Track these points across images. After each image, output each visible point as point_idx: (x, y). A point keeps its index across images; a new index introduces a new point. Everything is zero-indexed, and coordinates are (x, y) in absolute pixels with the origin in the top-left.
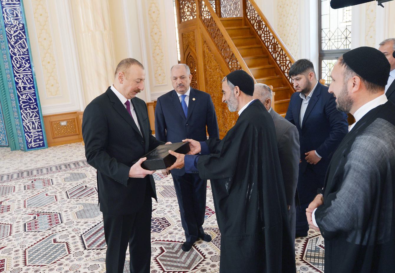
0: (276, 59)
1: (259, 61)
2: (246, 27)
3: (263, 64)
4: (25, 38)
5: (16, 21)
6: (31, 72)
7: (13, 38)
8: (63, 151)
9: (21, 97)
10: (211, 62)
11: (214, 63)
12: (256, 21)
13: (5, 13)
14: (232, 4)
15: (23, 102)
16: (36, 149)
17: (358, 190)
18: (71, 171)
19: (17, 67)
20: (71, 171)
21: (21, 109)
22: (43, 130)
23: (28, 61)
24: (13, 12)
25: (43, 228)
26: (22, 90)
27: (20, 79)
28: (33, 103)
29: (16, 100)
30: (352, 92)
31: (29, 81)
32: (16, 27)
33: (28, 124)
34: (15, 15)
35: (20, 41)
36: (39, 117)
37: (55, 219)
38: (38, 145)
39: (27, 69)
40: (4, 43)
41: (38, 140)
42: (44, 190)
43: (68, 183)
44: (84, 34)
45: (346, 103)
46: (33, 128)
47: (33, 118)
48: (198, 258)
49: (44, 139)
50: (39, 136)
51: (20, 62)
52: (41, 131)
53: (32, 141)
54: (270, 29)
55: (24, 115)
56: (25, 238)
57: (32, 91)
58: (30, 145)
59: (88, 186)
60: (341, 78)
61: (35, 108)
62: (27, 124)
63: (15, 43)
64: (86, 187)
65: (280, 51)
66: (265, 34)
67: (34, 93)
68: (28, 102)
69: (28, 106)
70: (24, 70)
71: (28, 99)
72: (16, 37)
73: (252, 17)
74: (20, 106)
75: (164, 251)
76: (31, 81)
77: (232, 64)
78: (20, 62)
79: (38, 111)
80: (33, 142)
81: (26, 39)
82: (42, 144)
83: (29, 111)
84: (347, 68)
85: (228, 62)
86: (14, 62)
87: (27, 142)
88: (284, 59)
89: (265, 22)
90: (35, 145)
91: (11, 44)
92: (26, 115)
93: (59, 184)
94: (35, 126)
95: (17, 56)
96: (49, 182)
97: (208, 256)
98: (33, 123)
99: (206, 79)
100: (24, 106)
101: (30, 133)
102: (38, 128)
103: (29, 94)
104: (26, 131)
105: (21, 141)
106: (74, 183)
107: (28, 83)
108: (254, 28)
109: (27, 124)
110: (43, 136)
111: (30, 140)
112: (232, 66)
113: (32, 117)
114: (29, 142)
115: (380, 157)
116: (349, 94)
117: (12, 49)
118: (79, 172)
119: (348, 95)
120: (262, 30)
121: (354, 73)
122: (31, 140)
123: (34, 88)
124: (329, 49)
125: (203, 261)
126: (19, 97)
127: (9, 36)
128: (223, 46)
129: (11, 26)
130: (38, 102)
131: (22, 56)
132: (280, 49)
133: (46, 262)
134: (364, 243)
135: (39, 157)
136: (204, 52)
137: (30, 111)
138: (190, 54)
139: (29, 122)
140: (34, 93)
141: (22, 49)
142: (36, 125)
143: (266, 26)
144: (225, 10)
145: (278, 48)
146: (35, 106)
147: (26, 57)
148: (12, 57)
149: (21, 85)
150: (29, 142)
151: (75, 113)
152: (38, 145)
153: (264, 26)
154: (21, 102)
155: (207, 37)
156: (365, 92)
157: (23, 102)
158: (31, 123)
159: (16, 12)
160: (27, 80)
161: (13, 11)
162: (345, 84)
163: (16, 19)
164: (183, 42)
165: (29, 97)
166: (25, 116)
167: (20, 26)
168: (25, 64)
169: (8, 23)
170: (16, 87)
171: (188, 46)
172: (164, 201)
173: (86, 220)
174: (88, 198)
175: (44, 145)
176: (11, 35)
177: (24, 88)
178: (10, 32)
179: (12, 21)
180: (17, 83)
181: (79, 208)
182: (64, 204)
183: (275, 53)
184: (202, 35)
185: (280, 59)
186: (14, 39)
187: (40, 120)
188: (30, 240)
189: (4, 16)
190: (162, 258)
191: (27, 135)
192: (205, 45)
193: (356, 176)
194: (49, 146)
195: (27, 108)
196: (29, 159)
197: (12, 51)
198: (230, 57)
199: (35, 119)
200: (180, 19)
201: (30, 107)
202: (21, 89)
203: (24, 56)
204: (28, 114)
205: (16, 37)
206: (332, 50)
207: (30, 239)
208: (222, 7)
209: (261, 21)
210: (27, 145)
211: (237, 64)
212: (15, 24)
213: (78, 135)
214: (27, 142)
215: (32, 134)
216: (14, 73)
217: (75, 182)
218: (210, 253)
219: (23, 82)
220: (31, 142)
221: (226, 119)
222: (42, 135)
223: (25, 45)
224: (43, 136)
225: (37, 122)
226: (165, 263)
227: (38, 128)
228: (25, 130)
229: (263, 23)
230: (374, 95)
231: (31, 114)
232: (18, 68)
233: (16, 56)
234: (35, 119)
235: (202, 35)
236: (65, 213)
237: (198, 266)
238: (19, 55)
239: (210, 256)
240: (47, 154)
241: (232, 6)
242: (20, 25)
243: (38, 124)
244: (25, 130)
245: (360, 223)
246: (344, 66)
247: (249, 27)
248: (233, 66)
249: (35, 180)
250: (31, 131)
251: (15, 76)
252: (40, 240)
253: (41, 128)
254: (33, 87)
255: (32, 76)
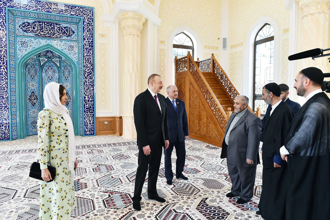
0: (230, 96)
1: (221, 96)
2: (214, 77)
3: (223, 98)
4: (93, 74)
5: (89, 65)
6: (93, 92)
7: (87, 73)
8: (105, 138)
9: (86, 106)
10: (194, 94)
11: (196, 95)
12: (220, 75)
13: (85, 60)
14: (206, 65)
15: (87, 108)
16: (89, 135)
17: (311, 126)
18: (112, 147)
19: (86, 89)
20: (112, 147)
21: (85, 112)
22: (95, 125)
23: (93, 86)
24: (89, 60)
25: (104, 171)
26: (87, 102)
27: (87, 95)
28: (91, 109)
29: (82, 107)
30: (305, 86)
31: (91, 97)
32: (89, 68)
33: (87, 121)
34: (90, 62)
35: (90, 75)
36: (94, 117)
37: (109, 168)
38: (90, 133)
39: (92, 91)
40: (81, 76)
41: (91, 131)
42: (99, 154)
43: (112, 153)
44: (126, 74)
45: (302, 91)
46: (89, 123)
47: (90, 118)
48: (196, 191)
49: (95, 130)
50: (92, 128)
51: (88, 86)
52: (94, 126)
53: (88, 131)
54: (228, 79)
55: (86, 115)
56: (30, 183)
57: (92, 103)
58: (86, 133)
59: (124, 154)
60: (300, 79)
61: (92, 112)
62: (86, 121)
63: (87, 76)
64: (123, 155)
65: (234, 91)
66: (224, 82)
67: (93, 104)
68: (89, 109)
69: (89, 111)
70: (90, 91)
71: (89, 107)
72: (88, 73)
73: (218, 72)
74: (85, 111)
75: (110, 197)
76: (92, 97)
77: (207, 95)
78: (88, 86)
79: (94, 114)
80: (88, 132)
81: (93, 74)
82: (92, 133)
83: (89, 114)
84: (303, 75)
85: (204, 95)
86: (85, 86)
87: (85, 131)
88: (234, 97)
89: (225, 75)
90: (89, 133)
91: (85, 76)
92: (87, 115)
93: (106, 152)
94: (91, 123)
95: (87, 83)
96: (101, 151)
97: (97, 208)
98: (90, 121)
99: (190, 104)
100: (86, 111)
101: (87, 126)
102: (92, 124)
103: (90, 104)
104: (85, 124)
105: (82, 130)
106: (116, 153)
107: (91, 98)
108: (219, 79)
109: (86, 121)
110: (94, 129)
111: (87, 130)
112: (207, 97)
113: (90, 117)
114: (86, 131)
115: (322, 112)
116: (304, 87)
117: (85, 79)
118: (117, 148)
119: (303, 87)
120: (223, 79)
121: (307, 77)
122: (88, 130)
123: (93, 101)
124: (259, 94)
125: (199, 192)
126: (85, 105)
127: (85, 72)
128: (202, 86)
129: (87, 67)
130: (94, 109)
131: (90, 83)
132: (233, 90)
133: (110, 186)
134: (312, 155)
135: (92, 139)
136: (190, 89)
137: (89, 114)
138: (181, 90)
139: (88, 120)
140: (93, 104)
141: (90, 80)
142: (92, 122)
143: (225, 78)
144: (201, 69)
145: (232, 89)
146: (92, 111)
147: (92, 84)
148: (84, 83)
149: (87, 99)
150: (86, 131)
151: (114, 117)
152: (90, 133)
153: (224, 77)
154: (85, 108)
155: (193, 80)
156: (311, 87)
157: (87, 108)
158: (89, 120)
159: (90, 60)
160: (90, 97)
161: (89, 59)
162: (302, 83)
163: (90, 64)
164: (177, 84)
165: (90, 106)
166: (86, 116)
167: (91, 67)
168: (91, 87)
169: (85, 65)
170: (84, 100)
171: (180, 86)
172: (145, 204)
173: (127, 170)
174: (125, 160)
175: (94, 134)
176: (86, 72)
177: (88, 101)
178: (86, 70)
179: (88, 64)
180: (85, 98)
181: (121, 164)
182: (112, 162)
183: (230, 92)
184: (190, 80)
185: (233, 96)
186: (87, 74)
187: (94, 119)
188: (98, 176)
189: (84, 62)
190: (175, 189)
191: (86, 127)
192: (191, 85)
193: (310, 120)
194: (96, 135)
195: (88, 112)
196: (86, 140)
197: (85, 80)
198: (206, 92)
199: (91, 119)
200: (177, 71)
201: (90, 112)
202: (86, 101)
203: (91, 83)
204: (88, 115)
205: (88, 73)
206: (260, 95)
207: (98, 175)
208: (200, 67)
209: (223, 75)
210: (85, 133)
211: (210, 95)
212: (89, 66)
213: (113, 130)
214: (85, 131)
215: (88, 127)
216: (84, 92)
217: (117, 152)
218: (202, 189)
219: (88, 97)
220: (87, 131)
221: (201, 127)
222: (94, 128)
223: (92, 77)
224: (94, 129)
225: (92, 120)
226: (177, 191)
227: (92, 124)
228: (85, 124)
229: (224, 76)
230: (316, 88)
231: (90, 116)
232: (87, 89)
233: (87, 83)
234: (91, 119)
235: (190, 80)
236: (91, 181)
237: (196, 194)
238: (88, 83)
239: (202, 190)
240: (96, 138)
241: (206, 66)
242: (91, 67)
243: (92, 122)
244: (85, 124)
245: (311, 142)
246: (302, 74)
247: (215, 78)
248: (207, 97)
249: (93, 150)
250: (88, 125)
251: (85, 94)
252: (104, 176)
253: (94, 124)
254: (93, 100)
255: (93, 94)
